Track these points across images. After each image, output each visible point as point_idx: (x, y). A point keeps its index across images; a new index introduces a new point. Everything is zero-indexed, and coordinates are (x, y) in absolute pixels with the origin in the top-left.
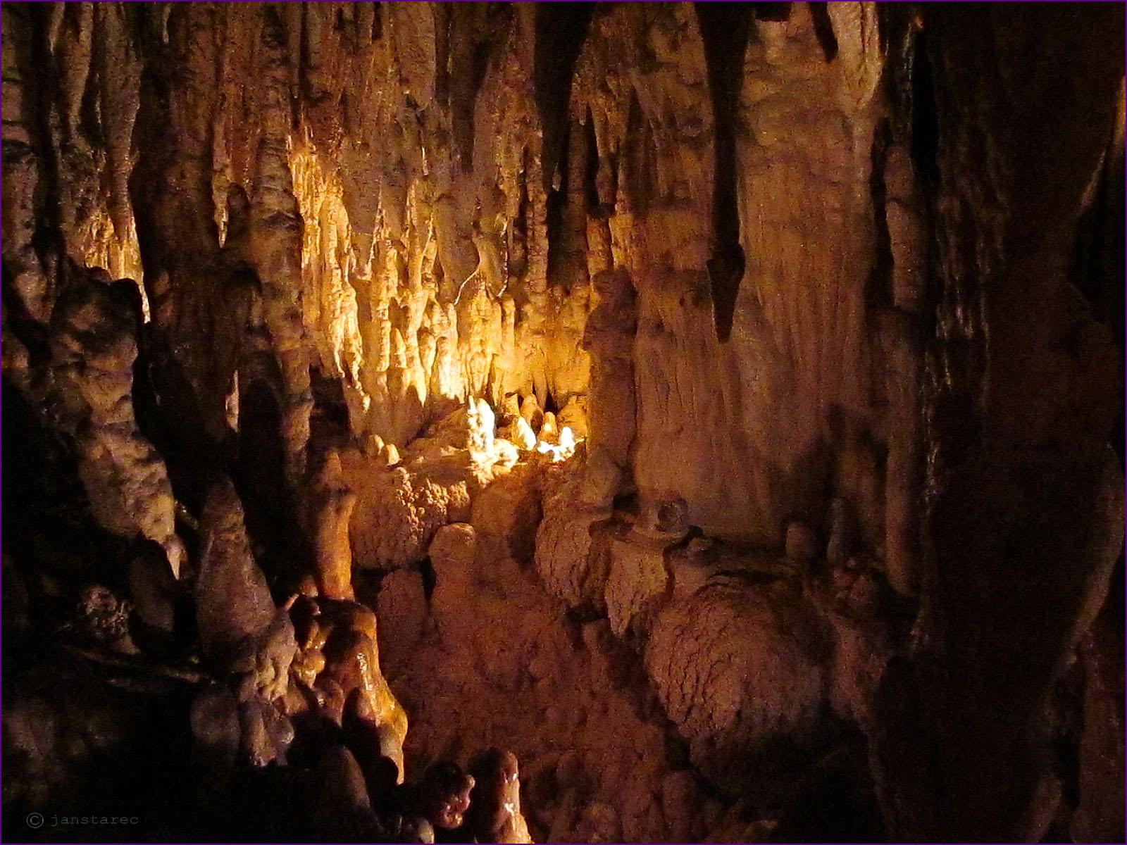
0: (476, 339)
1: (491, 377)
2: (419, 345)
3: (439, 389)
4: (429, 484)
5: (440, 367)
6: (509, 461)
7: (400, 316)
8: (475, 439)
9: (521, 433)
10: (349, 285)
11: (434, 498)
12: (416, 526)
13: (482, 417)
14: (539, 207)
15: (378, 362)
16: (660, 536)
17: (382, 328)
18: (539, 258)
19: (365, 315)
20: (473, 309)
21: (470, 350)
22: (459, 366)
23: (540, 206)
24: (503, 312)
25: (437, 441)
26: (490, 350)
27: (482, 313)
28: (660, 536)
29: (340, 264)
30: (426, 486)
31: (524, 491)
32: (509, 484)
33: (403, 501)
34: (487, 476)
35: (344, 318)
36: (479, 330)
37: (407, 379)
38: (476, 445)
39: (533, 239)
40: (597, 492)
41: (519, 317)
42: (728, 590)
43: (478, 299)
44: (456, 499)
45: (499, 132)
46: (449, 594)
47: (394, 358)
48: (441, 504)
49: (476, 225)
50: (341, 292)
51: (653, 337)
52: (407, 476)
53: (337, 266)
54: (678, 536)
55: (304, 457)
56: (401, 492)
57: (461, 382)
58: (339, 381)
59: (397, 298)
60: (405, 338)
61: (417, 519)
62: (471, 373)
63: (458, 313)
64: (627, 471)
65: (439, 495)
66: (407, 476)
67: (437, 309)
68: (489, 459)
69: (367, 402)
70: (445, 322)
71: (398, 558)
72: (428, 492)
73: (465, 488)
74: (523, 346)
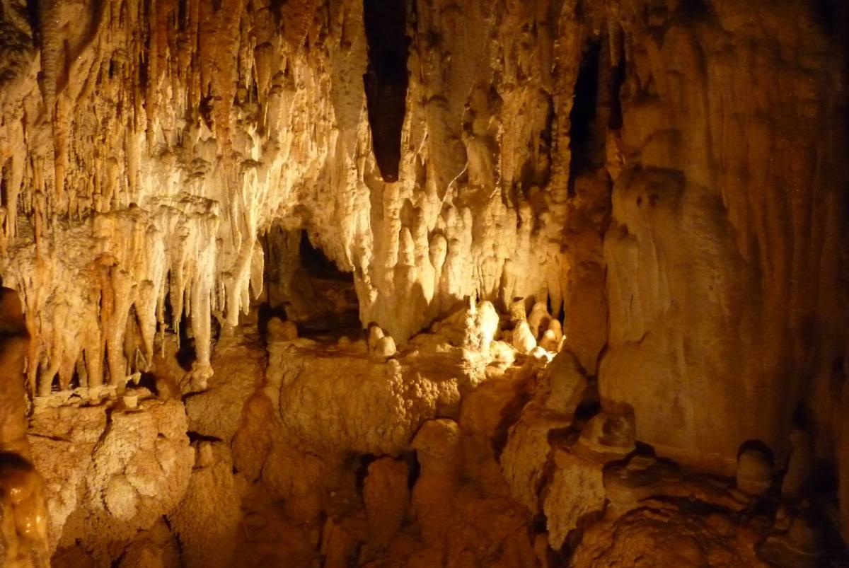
0: (488, 243)
1: (503, 280)
3: (447, 289)
5: (449, 267)
6: (504, 363)
7: (412, 216)
8: (471, 339)
9: (521, 338)
10: (364, 185)
11: (424, 392)
12: (402, 417)
13: (489, 319)
14: (563, 119)
16: (600, 449)
17: (393, 226)
18: (561, 168)
19: (378, 215)
20: (487, 214)
21: (482, 254)
23: (564, 117)
24: (519, 218)
25: (435, 338)
26: (502, 254)
27: (496, 219)
28: (600, 449)
29: (357, 165)
30: (417, 381)
31: (513, 394)
32: (498, 385)
33: (393, 392)
34: (480, 376)
35: (357, 215)
37: (414, 275)
38: (472, 344)
39: (556, 149)
40: (563, 398)
41: (537, 225)
42: (657, 517)
43: (493, 204)
44: (445, 394)
45: (494, 35)
46: (431, 486)
47: (403, 256)
48: (430, 399)
49: (468, 127)
50: (355, 191)
53: (354, 166)
54: (620, 451)
56: (392, 383)
57: (473, 284)
58: (351, 273)
59: (411, 200)
60: (415, 237)
63: (475, 218)
64: (591, 380)
65: (429, 390)
68: (483, 359)
69: (374, 295)
70: (461, 225)
72: (418, 385)
73: (456, 385)
74: (538, 253)
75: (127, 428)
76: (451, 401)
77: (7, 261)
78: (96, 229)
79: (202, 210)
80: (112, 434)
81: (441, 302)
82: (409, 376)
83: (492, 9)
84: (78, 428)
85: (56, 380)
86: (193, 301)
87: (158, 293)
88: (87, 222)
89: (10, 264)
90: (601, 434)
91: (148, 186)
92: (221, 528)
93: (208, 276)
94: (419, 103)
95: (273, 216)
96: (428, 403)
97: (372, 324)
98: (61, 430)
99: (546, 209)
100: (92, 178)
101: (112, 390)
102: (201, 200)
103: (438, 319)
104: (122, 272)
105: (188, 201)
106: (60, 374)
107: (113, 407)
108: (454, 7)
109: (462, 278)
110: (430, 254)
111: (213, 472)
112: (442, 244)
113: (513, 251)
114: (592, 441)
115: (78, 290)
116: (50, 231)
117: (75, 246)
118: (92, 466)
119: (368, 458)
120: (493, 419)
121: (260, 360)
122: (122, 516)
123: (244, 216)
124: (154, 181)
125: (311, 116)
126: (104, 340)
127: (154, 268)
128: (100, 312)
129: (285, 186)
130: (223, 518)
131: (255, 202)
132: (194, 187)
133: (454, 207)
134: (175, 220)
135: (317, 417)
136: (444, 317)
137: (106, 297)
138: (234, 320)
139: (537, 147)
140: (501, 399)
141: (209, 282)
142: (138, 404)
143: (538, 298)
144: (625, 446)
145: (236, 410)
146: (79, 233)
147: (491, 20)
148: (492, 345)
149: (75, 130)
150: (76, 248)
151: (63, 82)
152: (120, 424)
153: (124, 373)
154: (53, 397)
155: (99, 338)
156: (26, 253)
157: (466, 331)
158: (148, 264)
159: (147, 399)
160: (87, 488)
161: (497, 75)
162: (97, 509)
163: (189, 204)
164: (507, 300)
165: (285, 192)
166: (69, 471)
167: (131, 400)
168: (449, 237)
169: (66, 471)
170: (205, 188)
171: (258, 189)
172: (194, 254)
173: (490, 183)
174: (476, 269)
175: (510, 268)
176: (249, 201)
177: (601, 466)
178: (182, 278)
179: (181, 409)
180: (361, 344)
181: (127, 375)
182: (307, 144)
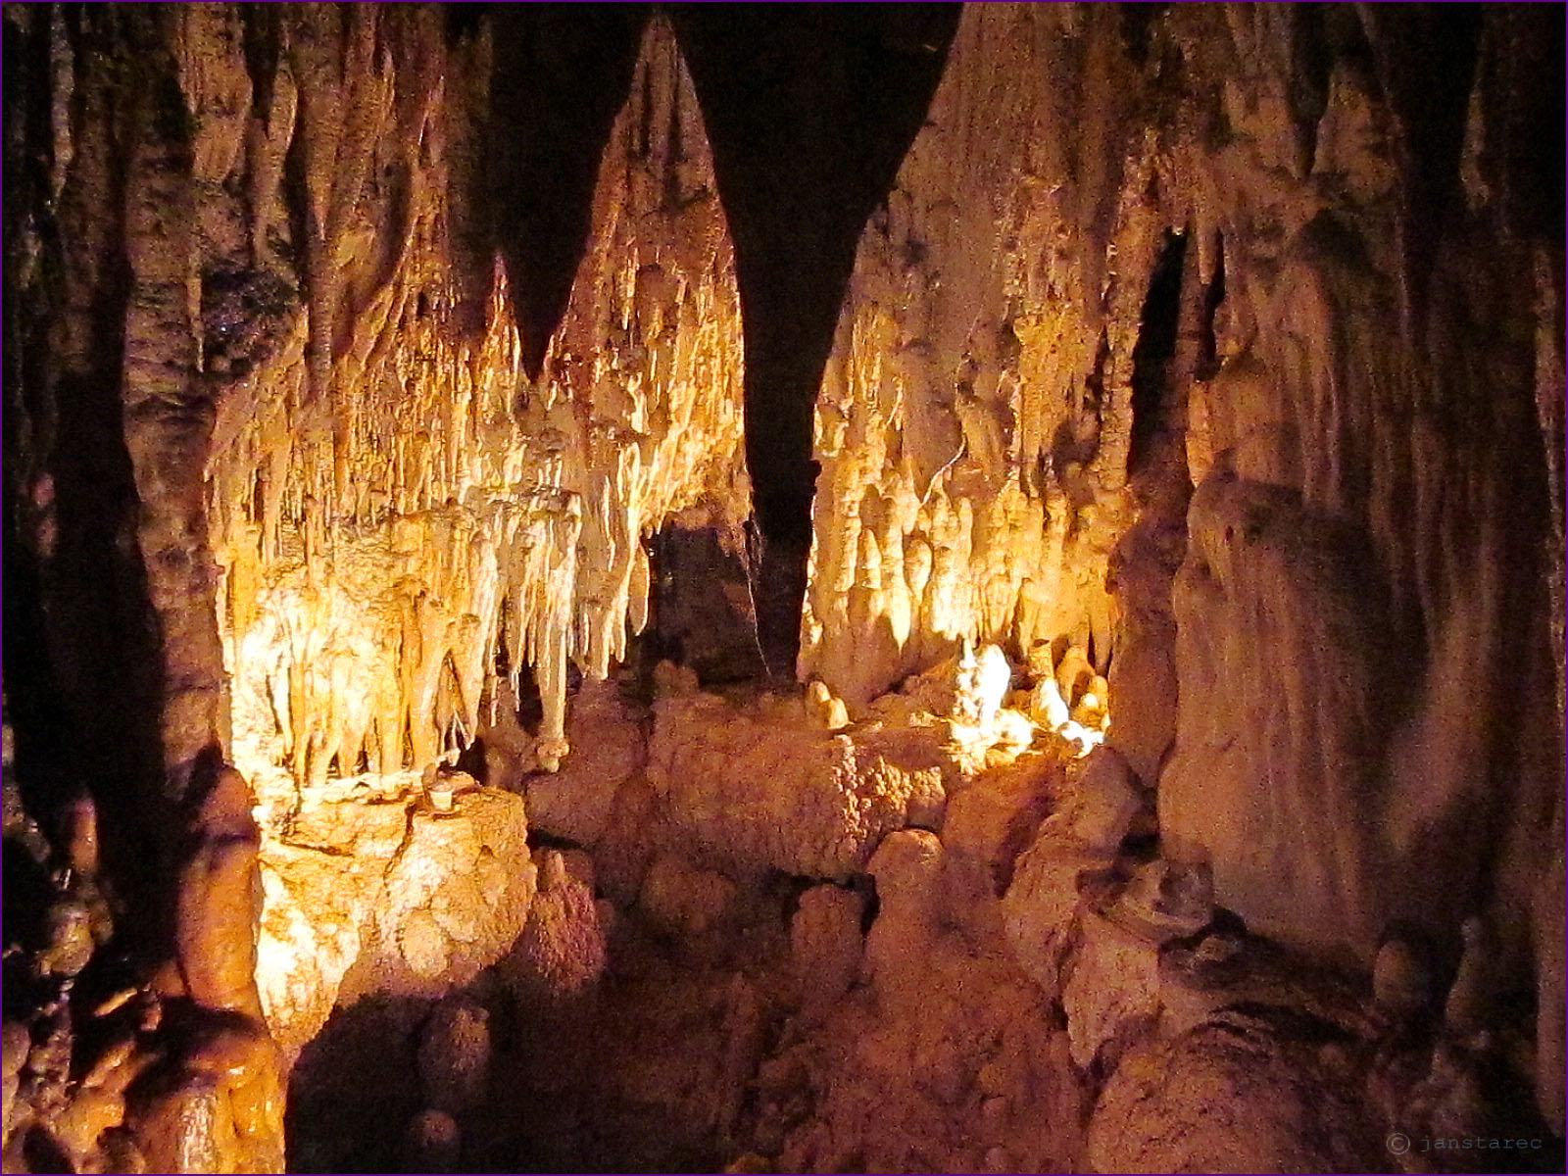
0: (998, 554)
2: (905, 557)
3: (931, 623)
4: (883, 765)
5: (934, 592)
8: (965, 706)
9: (1043, 707)
11: (888, 786)
13: (993, 672)
15: (837, 577)
16: (1156, 919)
18: (1116, 436)
20: (998, 507)
22: (970, 594)
24: (1046, 514)
26: (1018, 571)
27: (1010, 516)
28: (1156, 919)
30: (877, 767)
31: (1028, 794)
33: (841, 786)
36: (1003, 541)
37: (878, 605)
38: (967, 715)
39: (1109, 408)
40: (1097, 821)
41: (1075, 527)
45: (1011, 246)
46: (894, 933)
47: (862, 573)
48: (898, 800)
49: (965, 387)
51: (1192, 586)
52: (850, 749)
54: (1188, 925)
55: (187, 774)
56: (839, 772)
59: (878, 486)
60: (882, 543)
61: (857, 815)
62: (987, 604)
63: (976, 513)
64: (1146, 794)
65: (896, 784)
66: (850, 749)
67: (943, 504)
69: (816, 633)
70: (954, 524)
71: (828, 868)
72: (879, 777)
74: (1076, 569)
75: (435, 842)
76: (930, 802)
77: (264, 594)
78: (395, 539)
79: (556, 507)
80: (413, 849)
81: (921, 644)
82: (865, 761)
83: (1008, 206)
84: (365, 835)
85: (335, 761)
86: (540, 643)
87: (486, 631)
88: (384, 526)
89: (268, 598)
90: (1158, 896)
91: (473, 472)
92: (574, 982)
93: (563, 604)
94: (890, 349)
95: (665, 509)
96: (894, 804)
97: (813, 677)
98: (339, 838)
99: (1090, 500)
100: (391, 464)
101: (415, 778)
102: (554, 492)
103: (915, 671)
104: (433, 604)
105: (535, 494)
106: (340, 754)
107: (417, 806)
108: (947, 202)
109: (953, 607)
110: (906, 570)
111: (564, 898)
112: (925, 555)
113: (1036, 566)
114: (1141, 904)
115: (368, 632)
116: (328, 545)
117: (364, 565)
118: (384, 894)
119: (803, 883)
120: (995, 835)
121: (641, 723)
122: (425, 971)
123: (618, 515)
124: (483, 465)
125: (723, 364)
126: (405, 705)
127: (481, 596)
128: (400, 662)
129: (683, 466)
130: (579, 966)
131: (635, 495)
132: (544, 472)
133: (945, 496)
134: (513, 524)
135: (721, 816)
136: (918, 668)
137: (409, 642)
138: (601, 670)
139: (1080, 400)
140: (1005, 803)
141: (566, 614)
142: (454, 802)
143: (1073, 641)
144: (1195, 914)
145: (603, 800)
146: (372, 545)
147: (1006, 222)
148: (997, 716)
149: (367, 396)
150: (366, 569)
151: (343, 344)
152: (426, 834)
153: (435, 752)
154: (329, 789)
155: (397, 702)
156: (291, 579)
157: (957, 693)
158: (472, 590)
159: (466, 791)
160: (376, 926)
161: (1015, 302)
162: (390, 957)
163: (536, 498)
164: (1025, 642)
165: (683, 474)
166: (349, 903)
167: (442, 798)
168: (935, 544)
169: (345, 903)
170: (556, 474)
171: (640, 476)
172: (542, 571)
173: (999, 473)
174: (976, 592)
175: (1030, 591)
176: (627, 492)
177: (1155, 946)
178: (523, 610)
179: (518, 804)
180: (794, 706)
181: (439, 752)
182: (717, 402)
